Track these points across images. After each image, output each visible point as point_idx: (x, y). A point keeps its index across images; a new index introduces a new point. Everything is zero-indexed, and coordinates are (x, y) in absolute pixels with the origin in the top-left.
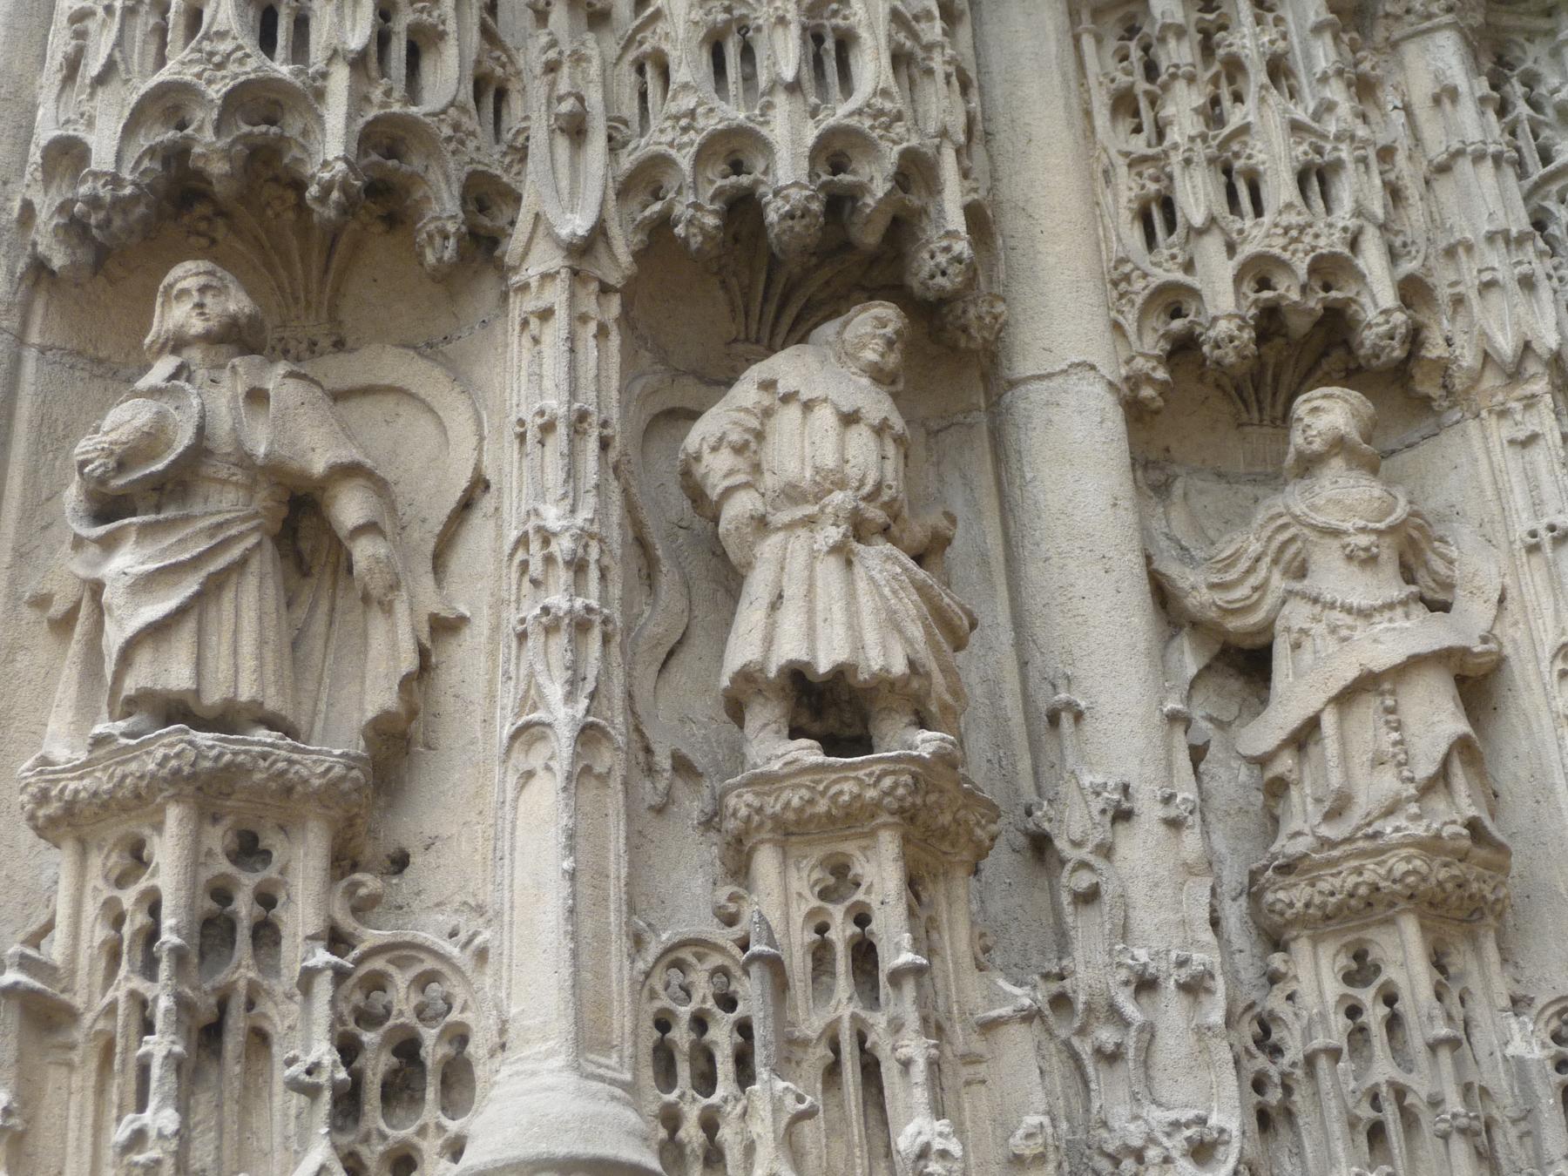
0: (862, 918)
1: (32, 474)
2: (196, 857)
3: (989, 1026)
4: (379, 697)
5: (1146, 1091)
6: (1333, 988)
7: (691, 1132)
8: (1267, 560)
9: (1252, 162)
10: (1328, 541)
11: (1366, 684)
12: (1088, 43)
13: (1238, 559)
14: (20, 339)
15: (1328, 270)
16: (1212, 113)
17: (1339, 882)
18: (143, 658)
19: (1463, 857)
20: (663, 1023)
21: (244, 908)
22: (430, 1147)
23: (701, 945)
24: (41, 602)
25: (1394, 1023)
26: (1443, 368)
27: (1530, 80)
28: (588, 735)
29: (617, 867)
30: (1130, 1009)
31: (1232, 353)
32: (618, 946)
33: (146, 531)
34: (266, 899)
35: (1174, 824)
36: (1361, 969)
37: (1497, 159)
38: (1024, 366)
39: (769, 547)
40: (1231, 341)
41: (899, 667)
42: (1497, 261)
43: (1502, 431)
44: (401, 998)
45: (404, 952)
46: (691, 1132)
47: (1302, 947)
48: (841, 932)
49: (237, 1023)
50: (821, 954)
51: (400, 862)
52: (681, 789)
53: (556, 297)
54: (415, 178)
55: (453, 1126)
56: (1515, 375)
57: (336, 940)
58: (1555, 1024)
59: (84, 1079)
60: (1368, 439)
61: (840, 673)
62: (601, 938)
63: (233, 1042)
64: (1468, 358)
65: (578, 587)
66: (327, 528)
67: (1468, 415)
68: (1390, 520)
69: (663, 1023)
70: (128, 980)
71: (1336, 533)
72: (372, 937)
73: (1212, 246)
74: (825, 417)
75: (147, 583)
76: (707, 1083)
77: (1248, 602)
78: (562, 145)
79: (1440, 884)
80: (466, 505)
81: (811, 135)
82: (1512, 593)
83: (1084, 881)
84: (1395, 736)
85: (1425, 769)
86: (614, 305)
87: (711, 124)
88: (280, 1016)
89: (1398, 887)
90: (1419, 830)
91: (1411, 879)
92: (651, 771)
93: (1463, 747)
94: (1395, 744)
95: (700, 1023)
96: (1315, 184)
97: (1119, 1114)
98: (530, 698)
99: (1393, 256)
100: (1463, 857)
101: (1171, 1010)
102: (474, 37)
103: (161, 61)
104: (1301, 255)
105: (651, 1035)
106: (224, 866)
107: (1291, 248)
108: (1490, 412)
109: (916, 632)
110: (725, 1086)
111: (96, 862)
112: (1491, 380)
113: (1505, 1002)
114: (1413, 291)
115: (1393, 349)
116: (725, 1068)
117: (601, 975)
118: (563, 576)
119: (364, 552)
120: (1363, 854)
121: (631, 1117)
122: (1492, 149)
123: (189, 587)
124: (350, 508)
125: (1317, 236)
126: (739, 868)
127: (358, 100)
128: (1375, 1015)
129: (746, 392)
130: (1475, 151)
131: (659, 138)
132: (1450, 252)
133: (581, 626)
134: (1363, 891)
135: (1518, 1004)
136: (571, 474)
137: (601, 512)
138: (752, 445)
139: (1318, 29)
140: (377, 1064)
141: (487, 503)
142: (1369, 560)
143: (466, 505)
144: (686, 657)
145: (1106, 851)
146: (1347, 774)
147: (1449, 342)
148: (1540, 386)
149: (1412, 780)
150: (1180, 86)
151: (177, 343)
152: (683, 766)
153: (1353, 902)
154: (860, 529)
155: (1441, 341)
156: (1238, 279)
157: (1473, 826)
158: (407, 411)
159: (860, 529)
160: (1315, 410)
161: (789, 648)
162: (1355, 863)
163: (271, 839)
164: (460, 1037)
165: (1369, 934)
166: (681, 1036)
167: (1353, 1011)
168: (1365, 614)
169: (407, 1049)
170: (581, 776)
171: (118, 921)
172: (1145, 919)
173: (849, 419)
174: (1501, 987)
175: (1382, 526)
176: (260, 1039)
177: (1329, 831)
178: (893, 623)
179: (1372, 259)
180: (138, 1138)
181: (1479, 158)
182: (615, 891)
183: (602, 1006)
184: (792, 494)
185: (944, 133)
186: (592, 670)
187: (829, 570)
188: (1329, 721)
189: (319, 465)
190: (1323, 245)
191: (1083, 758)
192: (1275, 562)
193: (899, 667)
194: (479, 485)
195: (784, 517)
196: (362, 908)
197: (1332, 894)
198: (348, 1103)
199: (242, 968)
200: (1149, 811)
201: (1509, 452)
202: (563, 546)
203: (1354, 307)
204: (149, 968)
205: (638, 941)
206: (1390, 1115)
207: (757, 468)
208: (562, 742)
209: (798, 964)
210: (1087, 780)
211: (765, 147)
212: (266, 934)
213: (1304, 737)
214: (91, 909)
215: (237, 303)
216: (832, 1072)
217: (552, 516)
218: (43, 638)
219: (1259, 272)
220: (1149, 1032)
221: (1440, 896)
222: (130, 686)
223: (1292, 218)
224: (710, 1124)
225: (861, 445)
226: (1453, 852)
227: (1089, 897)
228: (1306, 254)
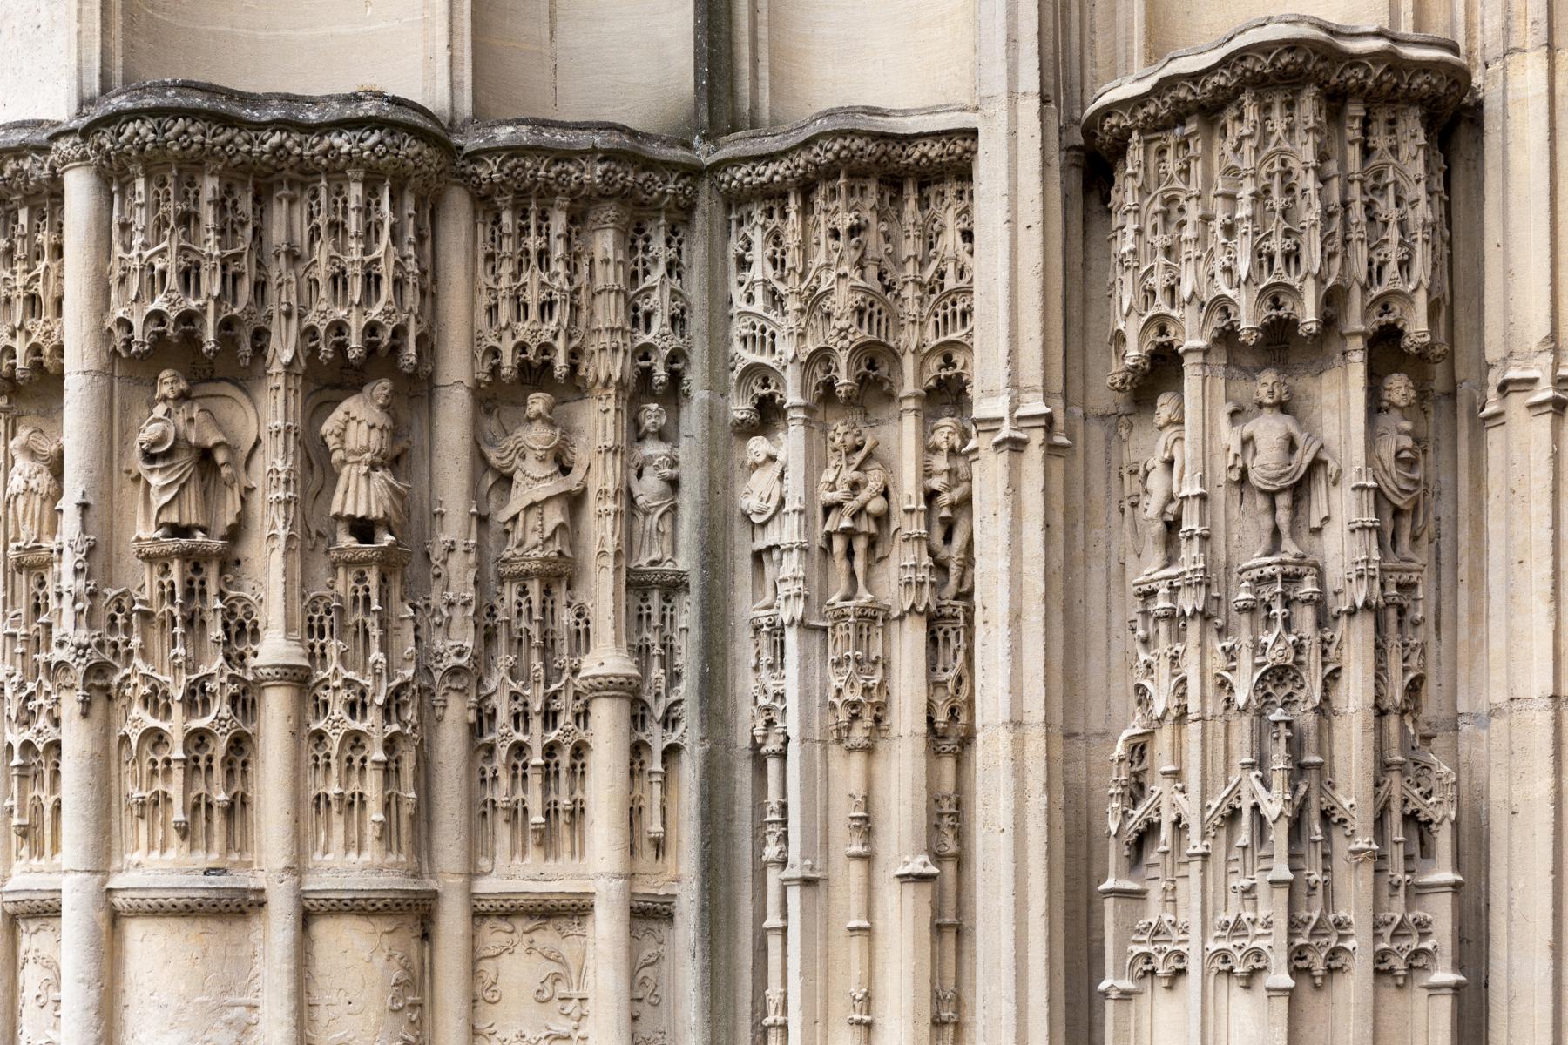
0: (367, 589)
1: (121, 425)
2: (183, 573)
3: (402, 620)
4: (230, 519)
5: (448, 636)
6: (515, 597)
7: (317, 650)
11: (533, 505)
12: (480, 226)
14: (112, 375)
15: (546, 349)
16: (516, 276)
17: (517, 568)
18: (165, 512)
20: (311, 619)
21: (196, 586)
22: (248, 653)
23: (322, 597)
24: (129, 472)
26: (584, 379)
27: (647, 239)
28: (290, 538)
29: (298, 577)
30: (445, 613)
32: (298, 599)
33: (162, 470)
34: (202, 583)
35: (467, 552)
36: (524, 592)
37: (618, 292)
38: (440, 382)
39: (346, 468)
41: (381, 515)
42: (605, 339)
44: (239, 610)
45: (240, 599)
46: (317, 650)
47: (507, 585)
48: (360, 594)
49: (197, 619)
50: (356, 599)
51: (238, 562)
52: (320, 541)
53: (280, 382)
54: (238, 335)
55: (254, 648)
56: (606, 386)
57: (222, 595)
59: (157, 632)
60: (550, 412)
61: (363, 518)
62: (293, 599)
63: (196, 625)
64: (591, 379)
65: (287, 489)
66: (215, 462)
69: (311, 619)
70: (167, 607)
72: (233, 593)
73: (507, 335)
74: (364, 426)
75: (164, 488)
76: (322, 636)
78: (283, 319)
80: (255, 446)
81: (363, 323)
83: (436, 571)
85: (547, 534)
86: (300, 380)
87: (331, 318)
88: (209, 617)
90: (540, 555)
92: (310, 537)
93: (561, 526)
95: (321, 619)
97: (438, 642)
98: (273, 527)
99: (570, 338)
101: (458, 612)
102: (254, 270)
103: (153, 300)
105: (307, 623)
106: (191, 575)
109: (387, 503)
110: (327, 637)
111: (155, 569)
112: (598, 386)
114: (574, 354)
116: (327, 632)
117: (293, 610)
118: (282, 486)
119: (225, 471)
121: (301, 650)
123: (175, 490)
124: (220, 457)
126: (335, 574)
127: (217, 311)
128: (525, 607)
129: (339, 414)
131: (312, 318)
133: (287, 502)
135: (569, 605)
136: (286, 449)
137: (294, 462)
138: (341, 436)
139: (559, 237)
140: (234, 630)
141: (261, 448)
142: (542, 460)
143: (255, 446)
144: (323, 494)
145: (445, 562)
148: (612, 391)
150: (506, 262)
151: (165, 399)
152: (319, 534)
154: (373, 467)
156: (514, 350)
157: (560, 553)
158: (236, 407)
159: (373, 467)
161: (349, 511)
163: (203, 565)
164: (256, 623)
166: (315, 623)
168: (538, 480)
169: (242, 625)
170: (288, 551)
171: (163, 587)
172: (454, 583)
173: (372, 427)
176: (203, 622)
177: (518, 552)
178: (379, 500)
179: (560, 344)
180: (176, 656)
181: (611, 291)
182: (297, 584)
183: (293, 619)
184: (354, 453)
185: (411, 311)
186: (291, 516)
187: (362, 481)
189: (210, 443)
191: (442, 530)
193: (381, 515)
194: (258, 441)
195: (351, 459)
196: (229, 585)
198: (226, 644)
199: (197, 605)
200: (460, 548)
202: (283, 476)
204: (172, 602)
205: (303, 597)
206: (524, 637)
207: (343, 441)
208: (282, 541)
209: (349, 602)
210: (442, 538)
211: (348, 326)
212: (203, 593)
213: (515, 518)
214: (155, 583)
215: (183, 385)
216: (356, 634)
217: (280, 465)
218: (130, 484)
219: (522, 347)
220: (450, 618)
222: (162, 519)
223: (536, 327)
224: (323, 647)
225: (375, 434)
227: (439, 576)
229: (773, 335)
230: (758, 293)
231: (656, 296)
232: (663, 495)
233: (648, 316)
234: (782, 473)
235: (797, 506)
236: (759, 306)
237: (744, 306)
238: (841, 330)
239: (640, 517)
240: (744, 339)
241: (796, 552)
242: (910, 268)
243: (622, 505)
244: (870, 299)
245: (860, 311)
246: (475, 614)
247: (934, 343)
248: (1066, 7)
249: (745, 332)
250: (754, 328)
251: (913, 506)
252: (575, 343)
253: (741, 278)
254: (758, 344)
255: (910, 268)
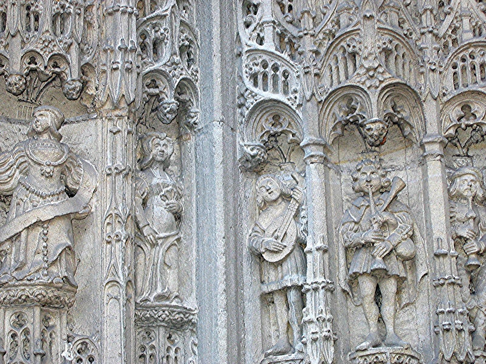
8: (15, 166)
9: (37, 9)
10: (36, 166)
11: (39, 223)
13: (5, 164)
19: (59, 289)
25: (27, 340)
31: (15, 89)
40: (15, 85)
43: (109, 126)
58: (79, 346)
67: (99, 117)
68: (59, 161)
71: (40, 164)
77: (6, 181)
79: (50, 298)
82: (99, 189)
84: (45, 244)
89: (36, 298)
91: (39, 297)
94: (44, 247)
96: (59, 19)
99: (82, 52)
100: (59, 289)
104: (47, 53)
107: (44, 50)
108: (106, 118)
112: (108, 106)
113: (65, 337)
114: (85, 68)
115: (73, 95)
120: (26, 285)
122: (129, 10)
125: (54, 46)
128: (21, 338)
130: (122, 10)
132: (105, 51)
134: (23, 297)
146: (26, 256)
147: (97, 89)
149: (47, 262)
153: (20, 300)
155: (94, 88)
160: (41, 115)
162: (23, 288)
165: (24, 310)
167: (14, 336)
174: (66, 332)
175: (57, 163)
179: (73, 56)
181: (124, 12)
188: (23, 234)
190: (56, 51)
192: (18, 168)
197: (14, 296)
201: (109, 135)
203: (64, 74)
221: (50, 301)
226: (56, 287)
228: (49, 53)
229: (285, 74)
230: (268, 33)
231: (165, 24)
232: (169, 228)
233: (156, 44)
234: (298, 211)
235: (319, 244)
236: (269, 45)
237: (255, 45)
238: (368, 70)
239: (147, 248)
240: (254, 77)
241: (322, 291)
242: (427, 20)
243: (131, 230)
244: (396, 42)
245: (387, 52)
246: (326, 305)
247: (456, 92)
248: (1, 183)
249: (256, 69)
250: (265, 66)
251: (445, 251)
252: (87, 59)
253: (248, 19)
254: (270, 82)
255: (427, 20)
